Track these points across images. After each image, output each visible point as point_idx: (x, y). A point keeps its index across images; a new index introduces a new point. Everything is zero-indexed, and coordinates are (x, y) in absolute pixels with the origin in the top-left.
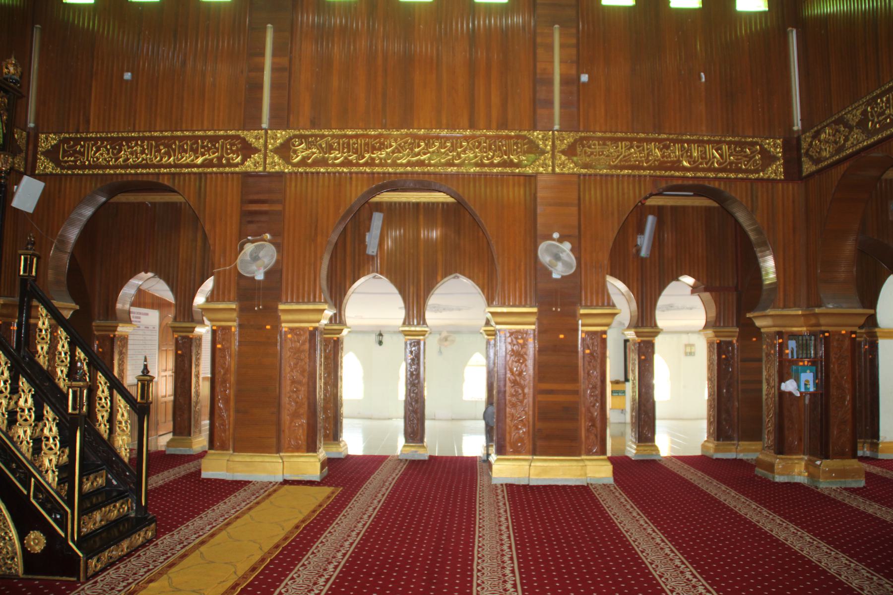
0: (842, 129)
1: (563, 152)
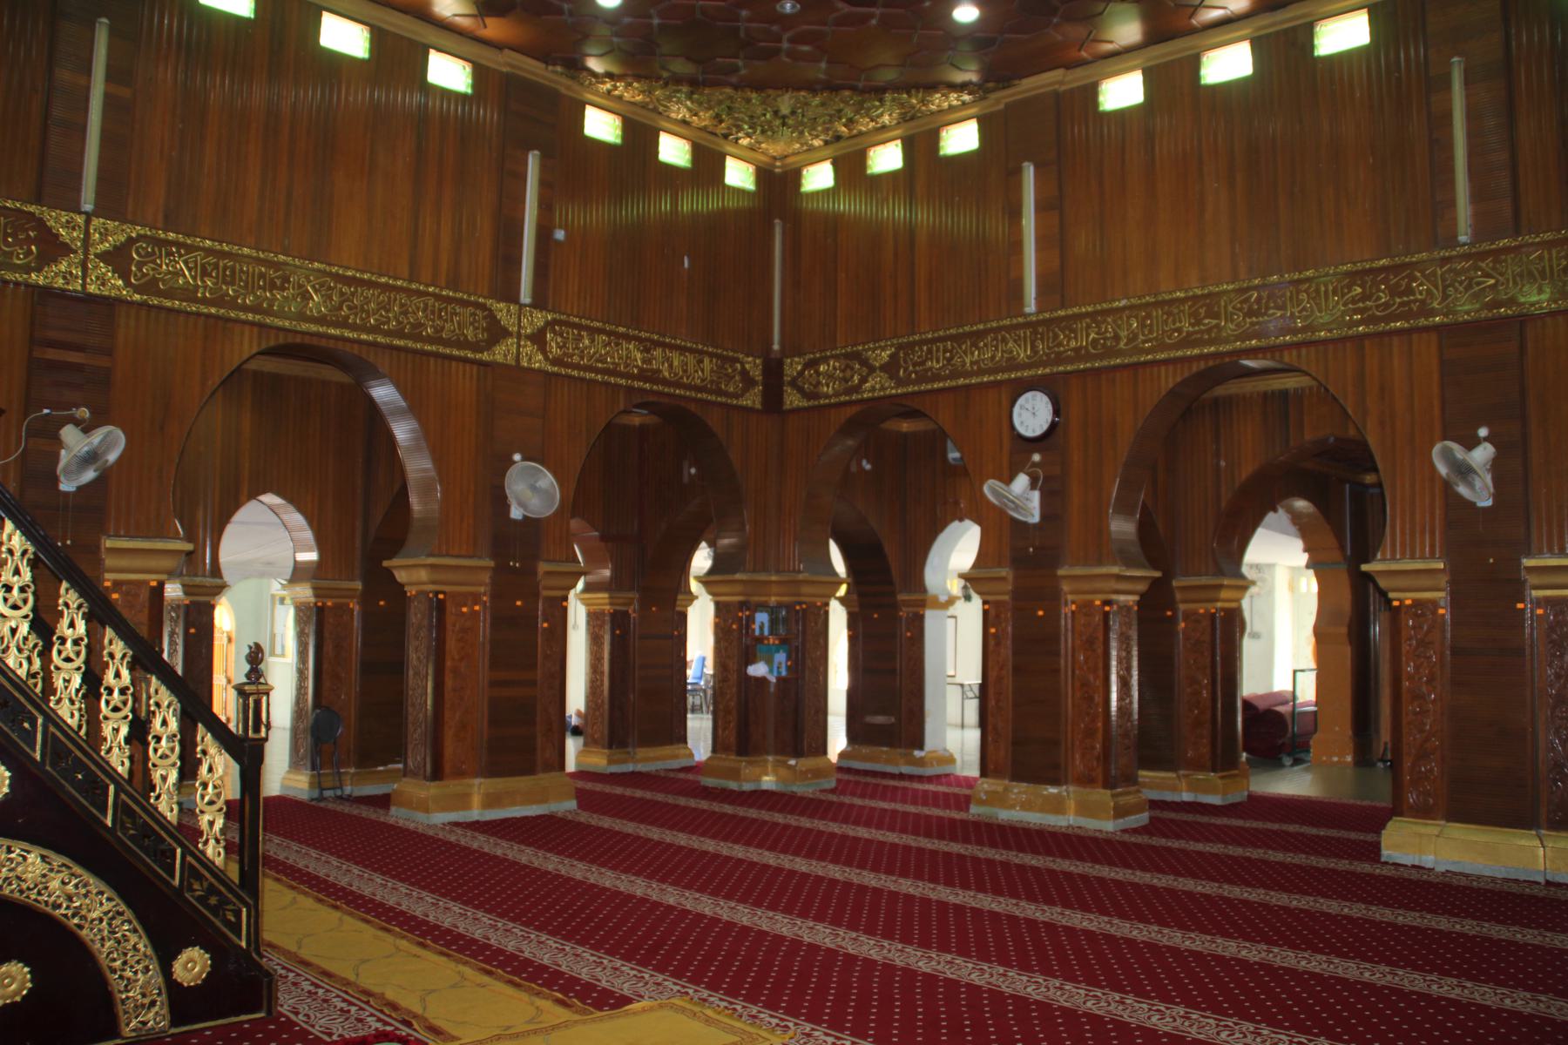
0: (857, 366)
1: (104, 257)
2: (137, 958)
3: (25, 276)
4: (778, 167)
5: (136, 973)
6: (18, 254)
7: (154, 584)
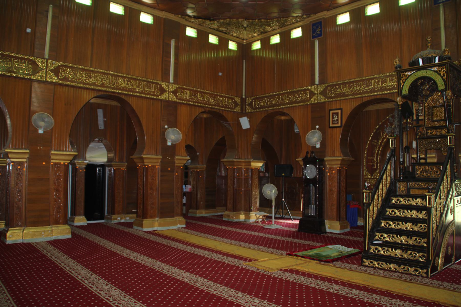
1: (52, 71)
4: (245, 42)
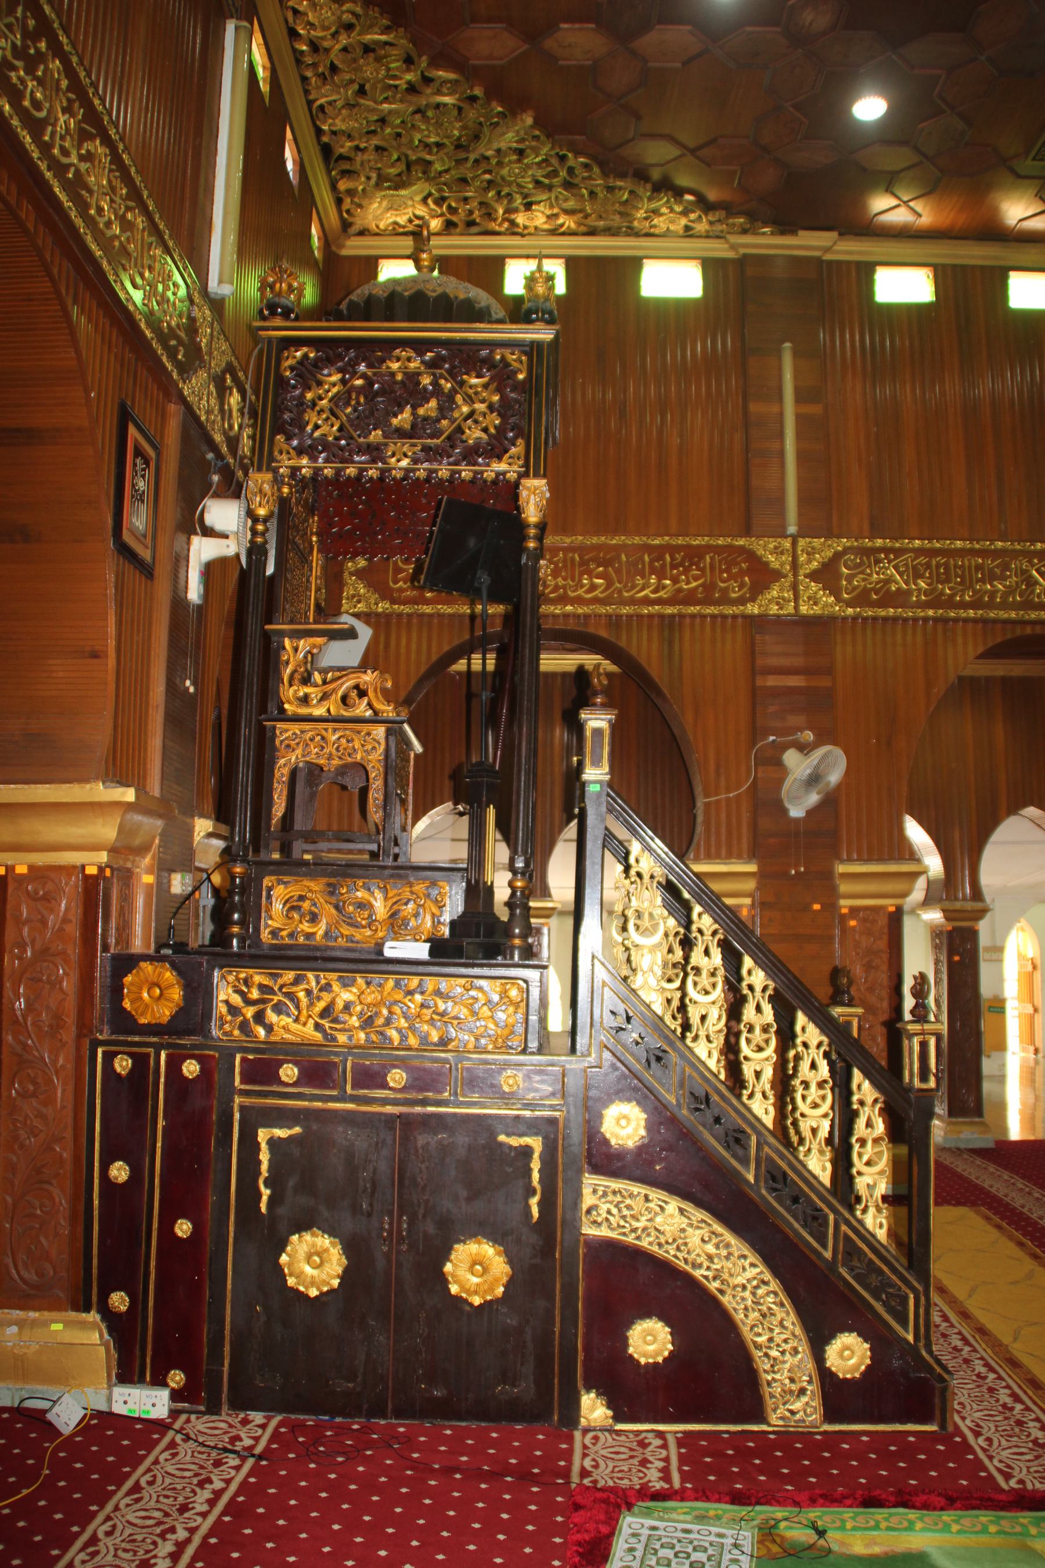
1: (814, 576)
2: (784, 1336)
3: (742, 608)
5: (783, 1353)
6: (734, 587)
7: (892, 909)
